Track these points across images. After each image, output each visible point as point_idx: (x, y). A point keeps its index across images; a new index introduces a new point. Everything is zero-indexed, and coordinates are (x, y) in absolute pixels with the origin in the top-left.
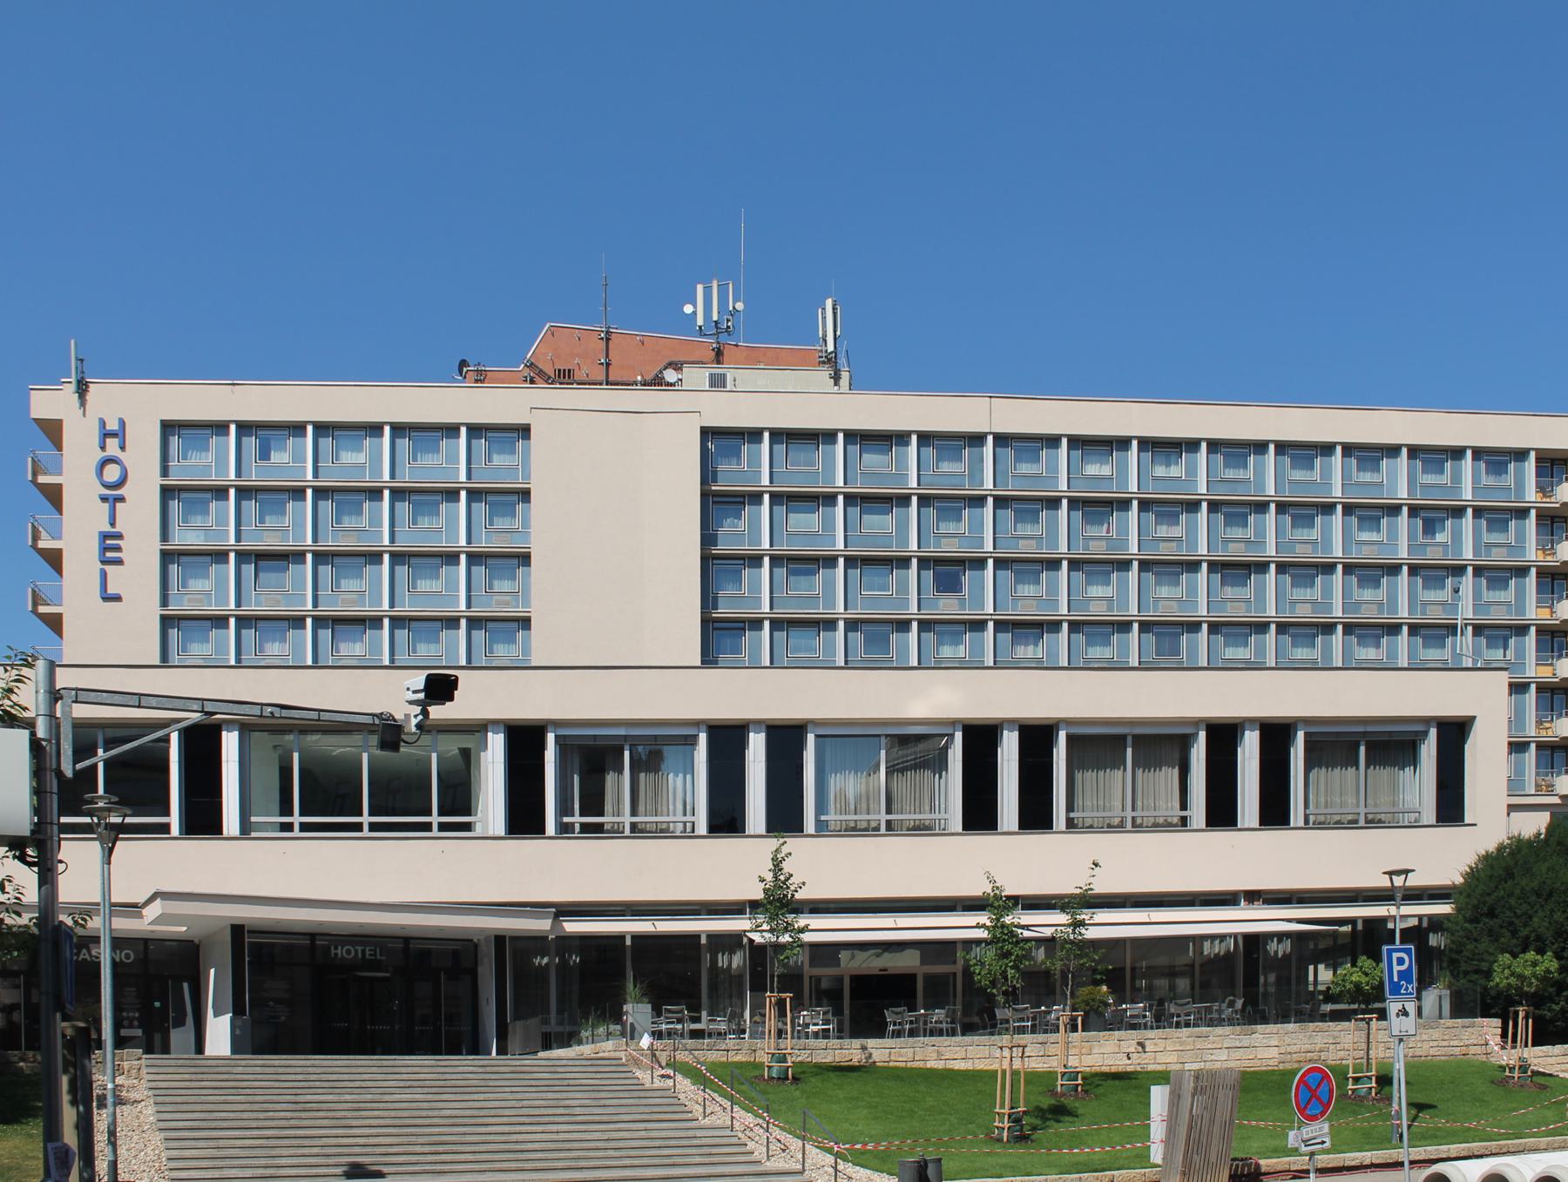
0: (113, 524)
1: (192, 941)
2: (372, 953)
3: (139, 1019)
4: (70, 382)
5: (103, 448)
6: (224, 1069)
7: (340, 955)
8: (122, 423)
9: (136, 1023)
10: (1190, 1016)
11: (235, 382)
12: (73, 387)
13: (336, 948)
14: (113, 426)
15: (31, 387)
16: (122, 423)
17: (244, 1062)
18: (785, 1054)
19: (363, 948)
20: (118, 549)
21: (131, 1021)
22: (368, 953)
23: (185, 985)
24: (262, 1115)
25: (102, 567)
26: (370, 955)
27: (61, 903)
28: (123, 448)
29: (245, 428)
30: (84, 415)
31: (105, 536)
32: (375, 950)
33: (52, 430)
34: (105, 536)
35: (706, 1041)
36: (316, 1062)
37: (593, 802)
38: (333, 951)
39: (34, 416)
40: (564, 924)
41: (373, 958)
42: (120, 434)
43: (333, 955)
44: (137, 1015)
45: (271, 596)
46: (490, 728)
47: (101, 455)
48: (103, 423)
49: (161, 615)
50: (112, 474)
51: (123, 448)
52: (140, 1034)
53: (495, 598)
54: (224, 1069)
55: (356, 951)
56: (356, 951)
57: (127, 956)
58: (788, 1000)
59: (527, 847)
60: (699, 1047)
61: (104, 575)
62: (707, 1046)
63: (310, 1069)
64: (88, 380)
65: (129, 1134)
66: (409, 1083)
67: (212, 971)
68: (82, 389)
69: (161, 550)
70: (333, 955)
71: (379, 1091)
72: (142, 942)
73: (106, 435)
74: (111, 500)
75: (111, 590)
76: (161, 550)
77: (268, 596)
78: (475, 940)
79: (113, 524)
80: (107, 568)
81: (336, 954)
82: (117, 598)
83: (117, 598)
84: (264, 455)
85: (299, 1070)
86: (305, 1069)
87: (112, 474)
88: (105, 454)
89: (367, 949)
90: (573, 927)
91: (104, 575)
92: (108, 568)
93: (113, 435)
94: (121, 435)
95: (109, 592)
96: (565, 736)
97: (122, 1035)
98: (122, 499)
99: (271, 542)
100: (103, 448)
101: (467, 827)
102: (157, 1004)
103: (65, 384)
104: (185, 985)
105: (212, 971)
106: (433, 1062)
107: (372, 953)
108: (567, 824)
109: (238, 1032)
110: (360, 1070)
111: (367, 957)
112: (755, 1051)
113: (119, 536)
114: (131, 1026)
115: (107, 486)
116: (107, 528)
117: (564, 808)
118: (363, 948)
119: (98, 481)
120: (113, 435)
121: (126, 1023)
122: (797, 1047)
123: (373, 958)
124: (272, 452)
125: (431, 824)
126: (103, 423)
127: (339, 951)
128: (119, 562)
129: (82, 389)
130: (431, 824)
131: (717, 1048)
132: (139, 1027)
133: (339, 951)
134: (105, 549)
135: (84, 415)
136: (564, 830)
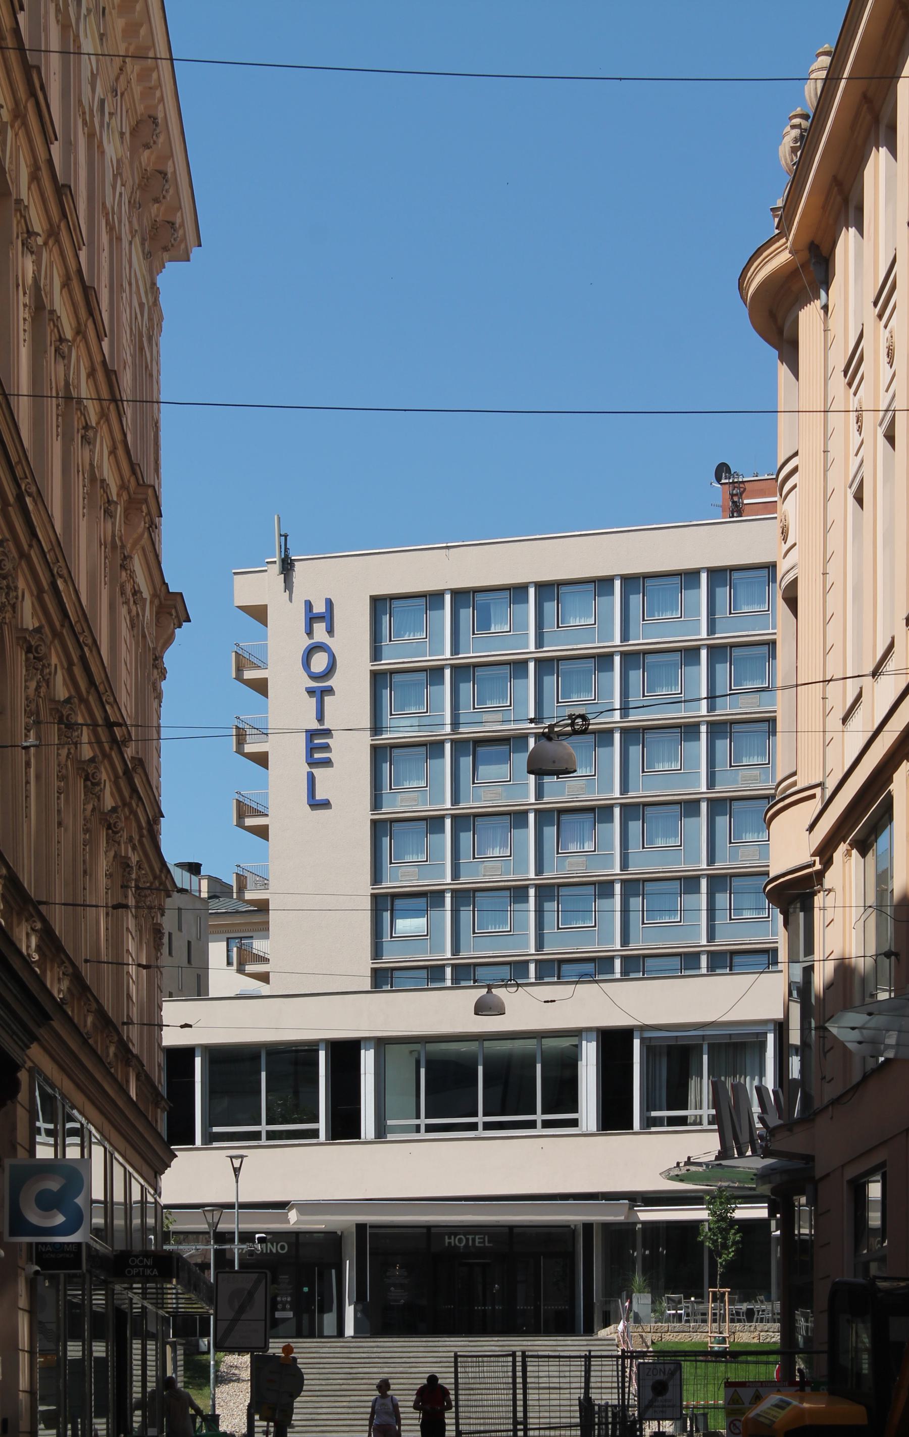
0: (320, 718)
1: (336, 1232)
2: (482, 1240)
3: (290, 1303)
4: (275, 562)
5: (310, 633)
6: (314, 1350)
7: (453, 1244)
8: (329, 604)
9: (288, 1306)
10: (686, 1320)
11: (449, 545)
12: (276, 568)
13: (450, 1238)
14: (319, 608)
15: (234, 571)
16: (329, 604)
17: (329, 1345)
18: (723, 1337)
19: (473, 1236)
20: (326, 748)
21: (284, 1304)
22: (477, 1241)
23: (333, 1271)
24: (323, 1382)
25: (310, 770)
26: (479, 1243)
27: (69, 1356)
28: (330, 631)
29: (461, 596)
30: (291, 600)
31: (312, 734)
32: (484, 1239)
33: (259, 613)
34: (312, 734)
35: (692, 1324)
36: (382, 1344)
37: (678, 1099)
38: (447, 1241)
39: (239, 602)
40: (639, 1214)
41: (482, 1245)
42: (328, 617)
43: (447, 1244)
44: (289, 1299)
45: (491, 788)
46: (584, 1034)
47: (306, 642)
48: (309, 605)
49: (372, 820)
50: (319, 662)
51: (330, 631)
52: (292, 1316)
53: (740, 773)
54: (314, 1350)
55: (467, 1239)
56: (467, 1239)
57: (282, 1248)
58: (727, 1293)
59: (617, 1142)
60: (686, 1329)
61: (311, 779)
62: (693, 1328)
63: (375, 1349)
64: (293, 558)
65: (238, 1394)
66: (439, 1360)
67: (348, 1262)
68: (287, 566)
69: (371, 745)
70: (447, 1244)
71: (408, 1365)
72: (294, 1235)
73: (312, 619)
74: (318, 693)
75: (319, 796)
76: (371, 745)
77: (487, 789)
78: (573, 1227)
79: (320, 718)
80: (314, 771)
81: (450, 1243)
82: (325, 804)
83: (325, 804)
84: (483, 623)
85: (366, 1350)
86: (371, 1349)
87: (319, 662)
88: (312, 641)
89: (477, 1237)
90: (648, 1215)
91: (311, 779)
92: (318, 772)
93: (320, 618)
94: (327, 618)
95: (318, 798)
96: (650, 1038)
97: (276, 1317)
98: (330, 691)
99: (492, 727)
100: (310, 633)
101: (574, 1123)
102: (306, 1289)
103: (269, 565)
104: (333, 1271)
105: (348, 1262)
106: (467, 1343)
107: (482, 1240)
108: (655, 1118)
109: (359, 1315)
110: (409, 1349)
111: (477, 1244)
112: (734, 1333)
113: (327, 733)
114: (284, 1309)
115: (314, 677)
116: (315, 725)
117: (649, 1104)
118: (473, 1236)
119: (305, 675)
120: (320, 618)
121: (280, 1306)
122: (771, 1330)
123: (482, 1245)
124: (363, 1052)
125: (535, 1121)
126: (309, 605)
127: (452, 1241)
128: (327, 763)
129: (287, 566)
130: (535, 1121)
131: (701, 1330)
132: (291, 1310)
133: (452, 1241)
134: (311, 749)
135: (291, 600)
136: (649, 1123)
